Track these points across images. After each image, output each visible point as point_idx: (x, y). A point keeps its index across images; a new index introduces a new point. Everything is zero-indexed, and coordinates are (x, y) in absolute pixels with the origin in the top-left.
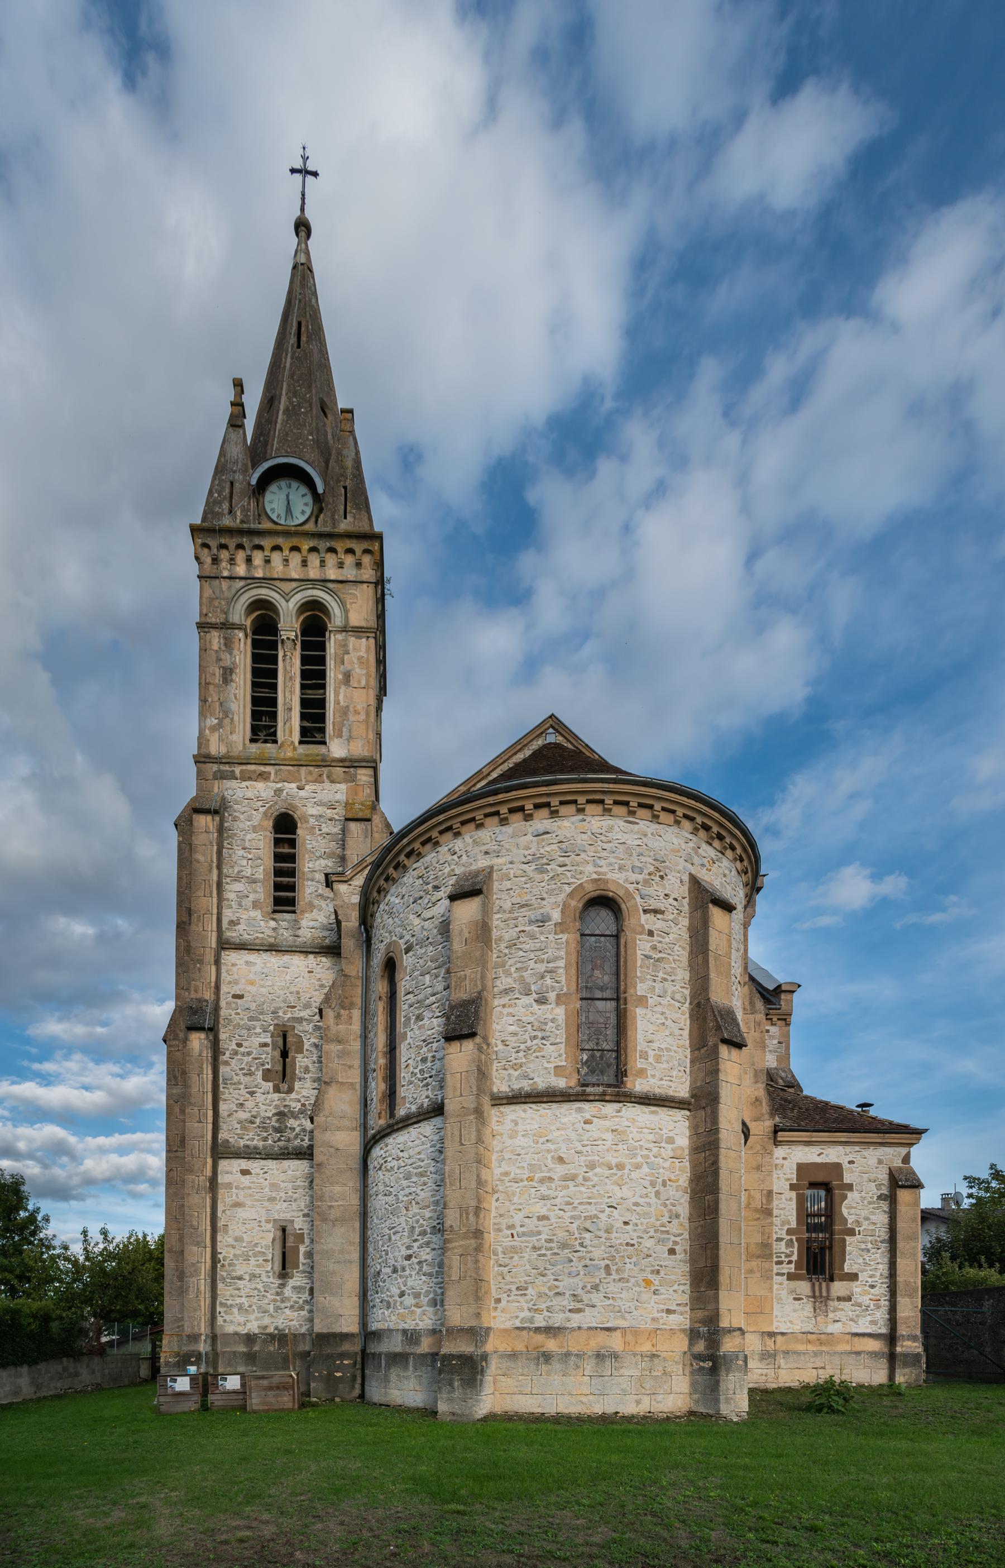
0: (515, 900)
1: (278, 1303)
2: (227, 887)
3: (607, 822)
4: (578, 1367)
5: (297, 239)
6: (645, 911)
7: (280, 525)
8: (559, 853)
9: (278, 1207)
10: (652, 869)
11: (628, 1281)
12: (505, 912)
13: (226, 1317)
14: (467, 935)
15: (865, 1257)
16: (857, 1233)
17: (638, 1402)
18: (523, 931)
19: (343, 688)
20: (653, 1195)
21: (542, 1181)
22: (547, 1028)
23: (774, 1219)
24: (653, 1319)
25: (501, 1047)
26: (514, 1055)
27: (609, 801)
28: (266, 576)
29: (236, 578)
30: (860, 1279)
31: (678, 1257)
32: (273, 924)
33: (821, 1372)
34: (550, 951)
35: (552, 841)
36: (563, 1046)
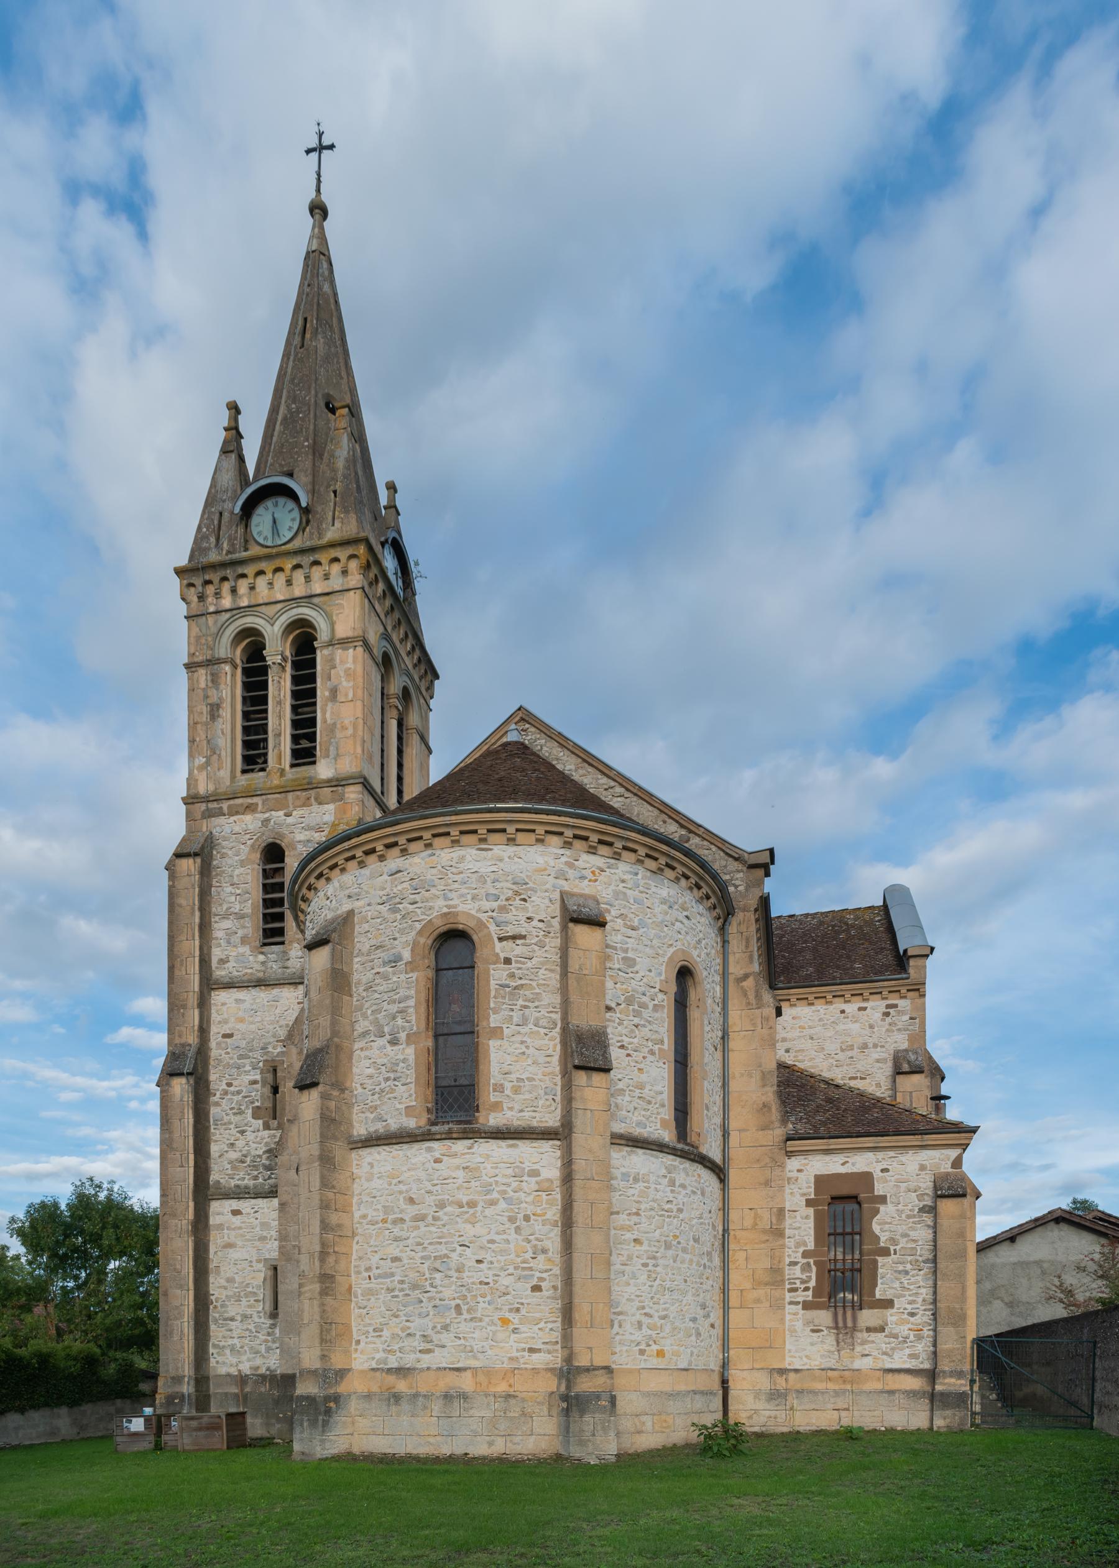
0: (373, 942)
1: (270, 1344)
2: (215, 926)
3: (458, 852)
4: (425, 1408)
5: (312, 220)
6: (501, 939)
7: (267, 547)
8: (410, 891)
9: (269, 1246)
10: (510, 893)
11: (481, 1320)
12: (363, 954)
13: (219, 1358)
14: (321, 984)
15: (903, 1280)
16: (892, 1252)
17: (490, 1444)
18: (378, 973)
19: (330, 705)
20: (513, 1231)
21: (395, 1222)
22: (399, 1069)
23: (787, 1240)
24: (511, 1359)
25: (360, 1090)
26: (370, 1098)
27: (454, 832)
28: (252, 604)
29: (221, 611)
30: (896, 1306)
31: (545, 1293)
32: (261, 958)
33: (844, 1414)
34: (401, 991)
35: (403, 880)
36: (412, 1086)
